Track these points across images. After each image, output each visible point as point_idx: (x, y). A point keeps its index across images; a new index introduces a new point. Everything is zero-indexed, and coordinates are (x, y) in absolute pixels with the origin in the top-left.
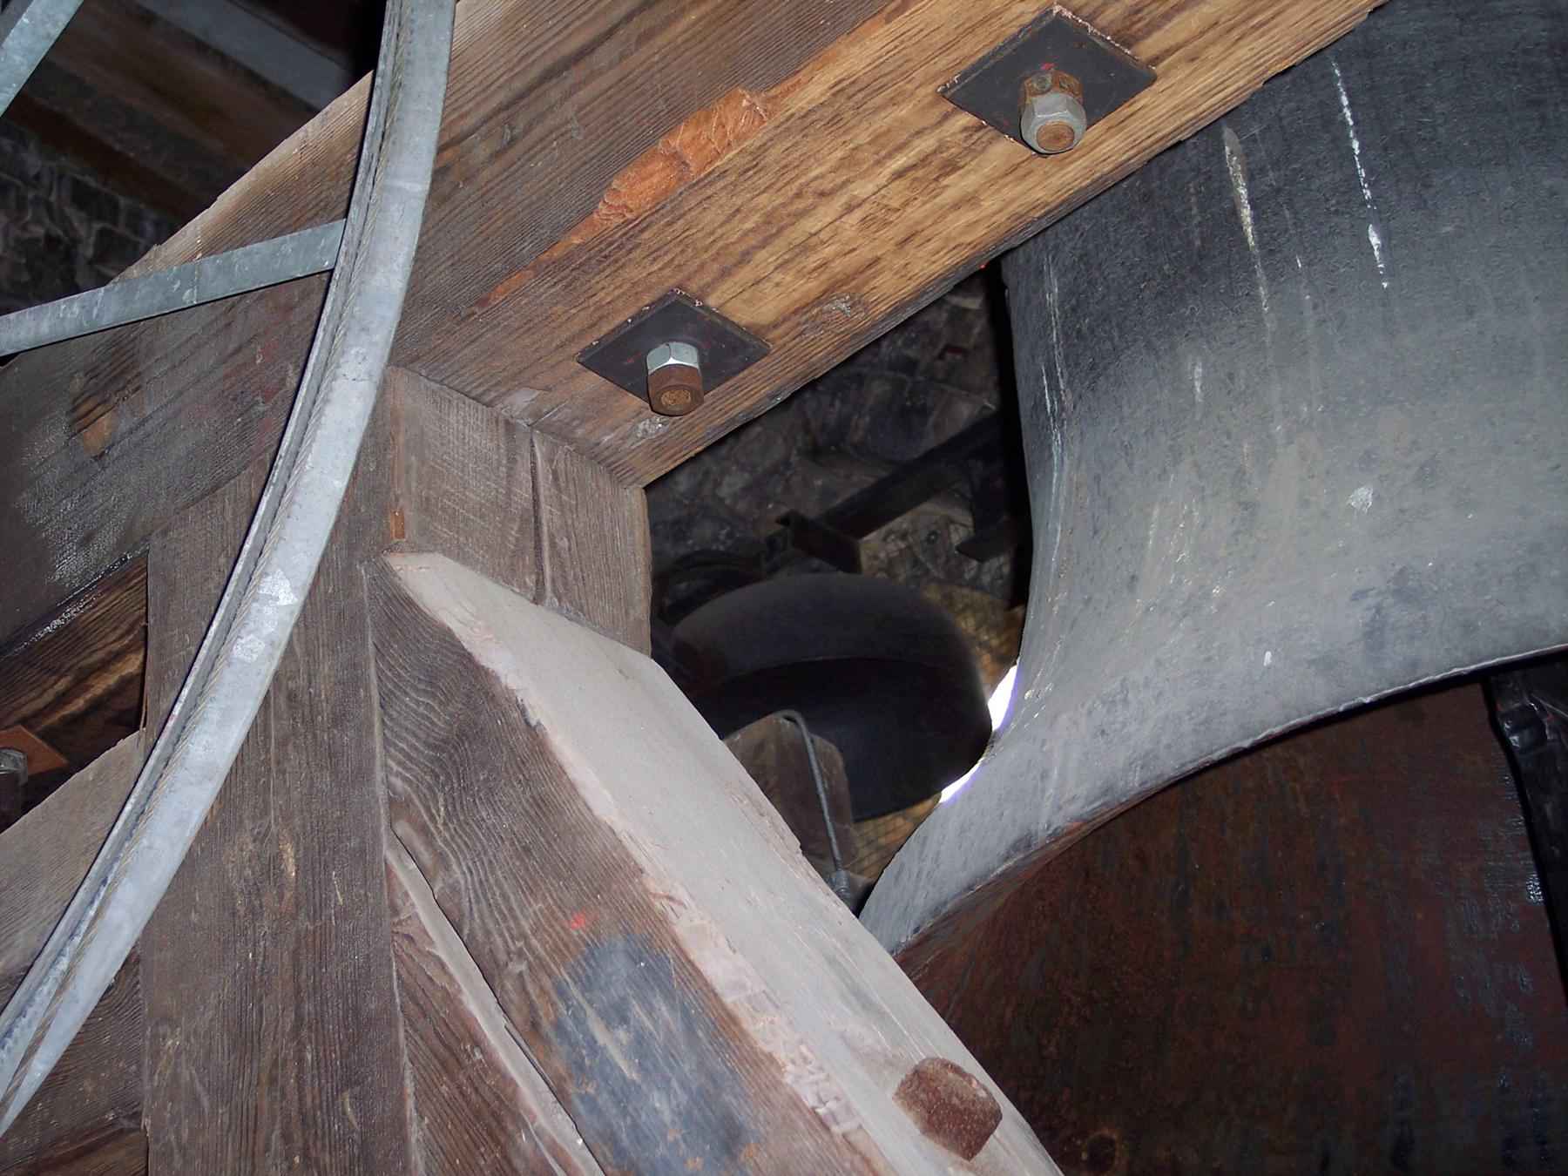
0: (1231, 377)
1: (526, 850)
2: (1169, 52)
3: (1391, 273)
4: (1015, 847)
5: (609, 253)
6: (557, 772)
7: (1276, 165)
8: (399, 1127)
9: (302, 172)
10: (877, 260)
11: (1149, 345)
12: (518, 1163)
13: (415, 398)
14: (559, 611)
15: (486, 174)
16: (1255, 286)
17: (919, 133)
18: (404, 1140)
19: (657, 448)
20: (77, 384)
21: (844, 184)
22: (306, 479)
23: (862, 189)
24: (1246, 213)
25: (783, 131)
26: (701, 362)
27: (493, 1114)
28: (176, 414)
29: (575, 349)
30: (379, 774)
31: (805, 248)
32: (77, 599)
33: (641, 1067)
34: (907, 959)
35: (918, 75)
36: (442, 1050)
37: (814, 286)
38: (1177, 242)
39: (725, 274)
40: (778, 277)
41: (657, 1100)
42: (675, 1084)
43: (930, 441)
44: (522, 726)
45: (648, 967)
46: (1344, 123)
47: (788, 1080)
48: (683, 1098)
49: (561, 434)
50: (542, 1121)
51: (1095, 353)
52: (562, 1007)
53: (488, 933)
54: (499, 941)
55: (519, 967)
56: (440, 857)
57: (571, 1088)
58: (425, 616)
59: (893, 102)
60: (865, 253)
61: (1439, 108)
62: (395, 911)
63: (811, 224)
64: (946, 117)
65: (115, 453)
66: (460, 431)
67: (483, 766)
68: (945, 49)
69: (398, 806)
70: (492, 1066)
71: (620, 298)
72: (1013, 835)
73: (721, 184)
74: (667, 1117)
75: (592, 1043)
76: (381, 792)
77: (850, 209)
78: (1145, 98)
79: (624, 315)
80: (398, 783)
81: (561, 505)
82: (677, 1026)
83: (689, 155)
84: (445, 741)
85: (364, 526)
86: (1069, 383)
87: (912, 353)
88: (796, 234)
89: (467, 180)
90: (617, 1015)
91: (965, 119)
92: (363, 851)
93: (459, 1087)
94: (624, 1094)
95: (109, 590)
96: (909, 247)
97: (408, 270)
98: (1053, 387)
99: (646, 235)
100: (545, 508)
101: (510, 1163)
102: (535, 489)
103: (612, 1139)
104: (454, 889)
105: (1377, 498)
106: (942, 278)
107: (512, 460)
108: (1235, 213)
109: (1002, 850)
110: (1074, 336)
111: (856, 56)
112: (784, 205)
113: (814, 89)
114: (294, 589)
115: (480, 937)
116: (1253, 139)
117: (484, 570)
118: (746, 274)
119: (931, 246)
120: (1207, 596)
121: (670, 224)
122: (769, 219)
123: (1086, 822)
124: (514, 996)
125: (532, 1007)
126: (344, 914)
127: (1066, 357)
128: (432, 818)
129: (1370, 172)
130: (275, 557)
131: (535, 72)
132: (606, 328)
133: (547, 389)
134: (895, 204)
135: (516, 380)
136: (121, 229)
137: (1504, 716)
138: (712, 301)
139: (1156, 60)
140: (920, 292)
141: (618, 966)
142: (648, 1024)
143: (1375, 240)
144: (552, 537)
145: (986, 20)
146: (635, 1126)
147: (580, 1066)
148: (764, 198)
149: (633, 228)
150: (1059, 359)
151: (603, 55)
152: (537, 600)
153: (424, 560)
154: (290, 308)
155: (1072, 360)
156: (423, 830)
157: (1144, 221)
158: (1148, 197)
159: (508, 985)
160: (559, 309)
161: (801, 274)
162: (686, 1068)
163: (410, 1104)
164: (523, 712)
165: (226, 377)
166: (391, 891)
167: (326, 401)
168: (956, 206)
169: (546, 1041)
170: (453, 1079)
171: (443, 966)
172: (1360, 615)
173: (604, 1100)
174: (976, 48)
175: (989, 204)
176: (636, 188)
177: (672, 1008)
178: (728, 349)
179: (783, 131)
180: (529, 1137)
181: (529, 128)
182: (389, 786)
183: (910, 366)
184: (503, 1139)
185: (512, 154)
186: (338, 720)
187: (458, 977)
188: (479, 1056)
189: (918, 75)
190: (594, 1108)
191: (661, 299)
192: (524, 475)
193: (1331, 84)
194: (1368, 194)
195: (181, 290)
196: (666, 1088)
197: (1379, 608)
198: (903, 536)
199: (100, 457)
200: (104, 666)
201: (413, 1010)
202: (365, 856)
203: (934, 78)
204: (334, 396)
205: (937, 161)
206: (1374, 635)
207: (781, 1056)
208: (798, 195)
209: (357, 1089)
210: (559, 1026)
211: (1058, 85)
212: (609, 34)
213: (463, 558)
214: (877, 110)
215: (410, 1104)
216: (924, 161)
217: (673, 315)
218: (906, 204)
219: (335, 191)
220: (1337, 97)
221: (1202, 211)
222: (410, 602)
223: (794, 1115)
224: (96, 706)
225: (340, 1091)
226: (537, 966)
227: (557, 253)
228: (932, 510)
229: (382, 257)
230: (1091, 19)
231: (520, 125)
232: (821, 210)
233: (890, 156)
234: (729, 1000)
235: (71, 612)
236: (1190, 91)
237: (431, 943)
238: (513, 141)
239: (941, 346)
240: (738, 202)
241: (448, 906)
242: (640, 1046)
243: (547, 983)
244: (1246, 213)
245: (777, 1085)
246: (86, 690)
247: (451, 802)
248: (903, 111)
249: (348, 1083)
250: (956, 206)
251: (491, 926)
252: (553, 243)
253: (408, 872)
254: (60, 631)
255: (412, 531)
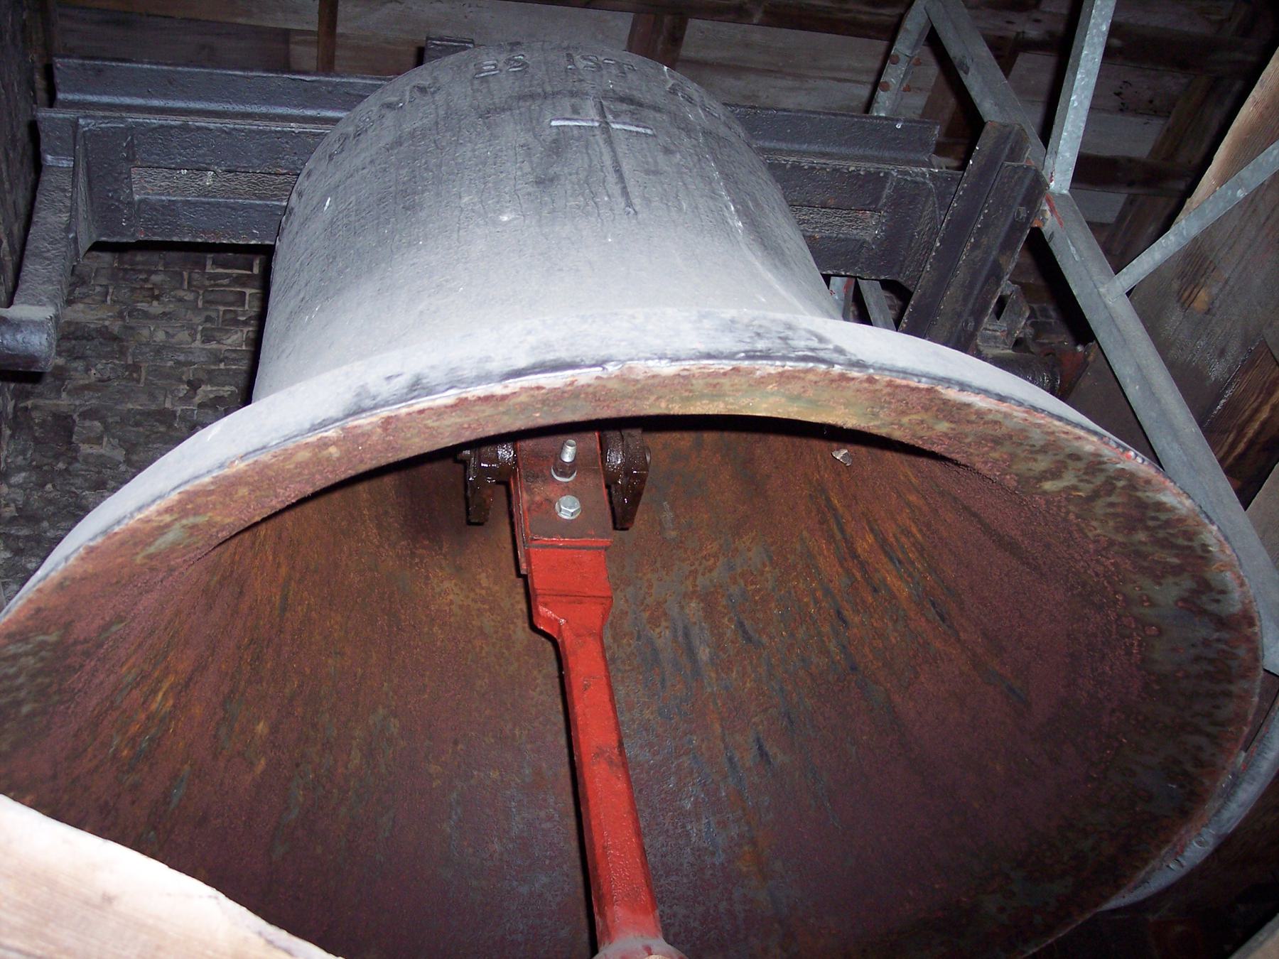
20: (1176, 286)
28: (1245, 268)
32: (1230, 384)
65: (1217, 304)
95: (1246, 372)
136: (1041, 319)
165: (1267, 235)
195: (1234, 194)
199: (1208, 312)
200: (1251, 418)
224: (1251, 443)
235: (1229, 393)
246: (1244, 436)
254: (1225, 406)
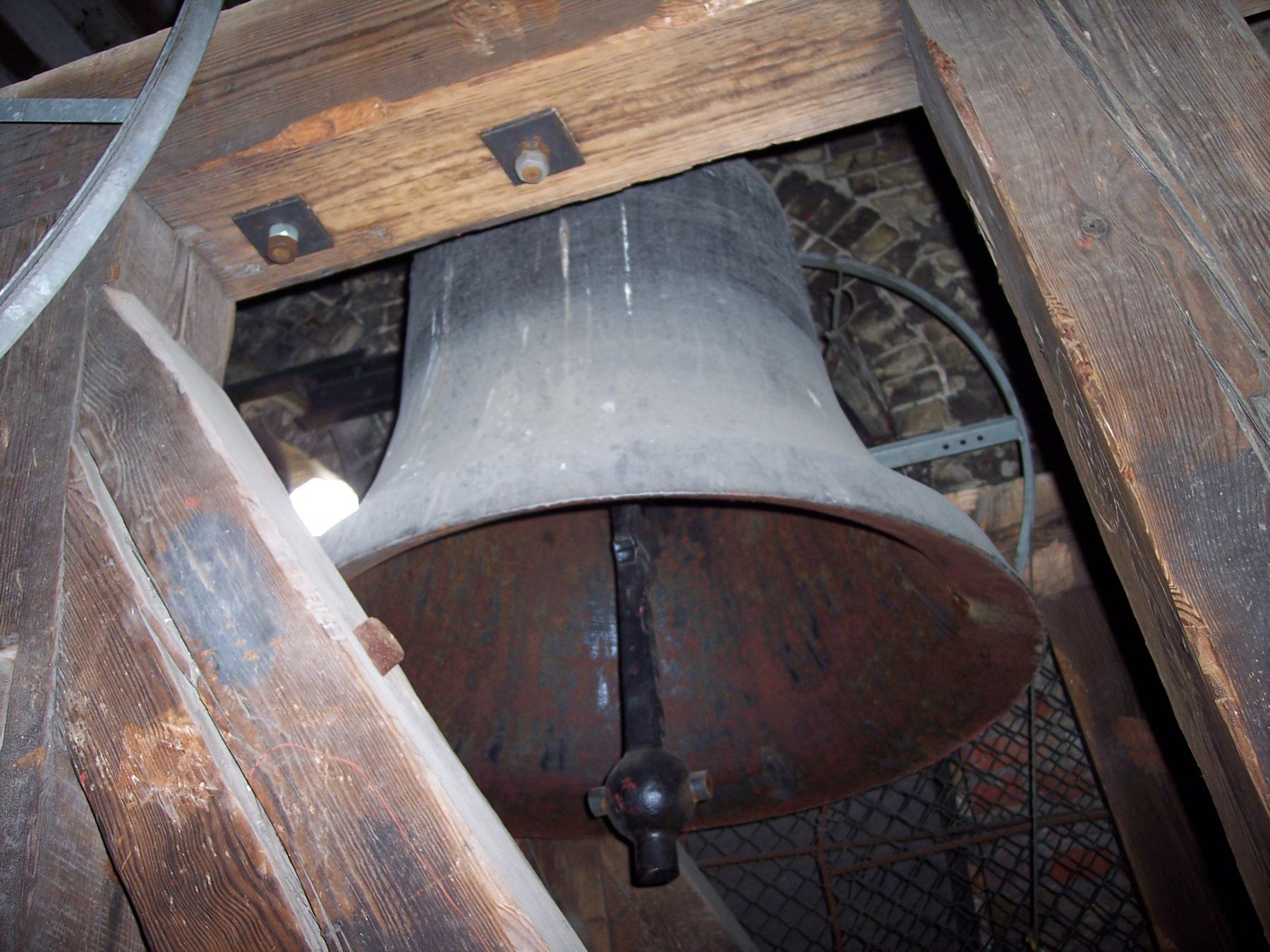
0: (544, 336)
1: (165, 458)
2: (595, 152)
3: (633, 308)
4: (407, 532)
5: (273, 163)
6: (193, 422)
7: (585, 243)
8: (50, 594)
9: (93, 76)
10: (408, 214)
11: (501, 313)
12: (127, 627)
13: (140, 212)
14: (185, 348)
15: (211, 104)
16: (563, 296)
17: (459, 152)
18: (53, 602)
19: (253, 281)
21: (411, 166)
22: (74, 229)
23: (418, 172)
24: (565, 262)
25: (392, 127)
26: (300, 237)
27: (115, 596)
29: (233, 211)
30: (76, 401)
31: (375, 195)
33: (217, 586)
34: (342, 571)
35: (472, 120)
36: (87, 556)
37: (370, 217)
38: (526, 266)
39: (329, 195)
40: (355, 206)
41: (224, 605)
42: (236, 598)
43: (291, 364)
44: (175, 392)
45: (231, 533)
46: (622, 233)
47: (308, 607)
48: (240, 606)
49: (204, 257)
50: (146, 604)
51: (468, 307)
52: (171, 546)
53: (131, 498)
54: (137, 504)
55: (146, 520)
56: (108, 454)
57: (169, 590)
58: (123, 323)
59: (453, 131)
60: (404, 208)
61: (669, 240)
62: (72, 476)
63: (384, 183)
64: (476, 148)
66: (157, 237)
67: (145, 409)
68: (492, 110)
69: (85, 420)
70: (119, 569)
71: (269, 189)
72: (406, 527)
73: (347, 145)
74: (228, 614)
75: (187, 568)
76: (75, 410)
77: (407, 181)
78: (573, 173)
79: (267, 201)
80: (88, 408)
81: (197, 295)
82: (243, 567)
83: (337, 123)
84: (124, 391)
85: (95, 269)
86: (450, 322)
87: (293, 318)
88: (373, 186)
89: (198, 104)
90: (207, 555)
91: (486, 152)
92: (56, 440)
93: (95, 579)
94: (202, 598)
96: (428, 212)
97: (162, 136)
98: (439, 322)
99: (297, 160)
100: (189, 294)
101: (121, 624)
102: (186, 282)
103: (191, 621)
104: (114, 471)
105: (617, 409)
106: (436, 235)
107: (178, 261)
108: (559, 259)
109: (398, 533)
110: (457, 300)
111: (446, 99)
112: (375, 167)
113: (417, 108)
114: (51, 287)
115: (126, 499)
116: (576, 228)
117: (154, 313)
118: (338, 199)
119: (438, 215)
120: (523, 434)
121: (313, 158)
122: (363, 173)
123: (450, 527)
124: (142, 535)
125: (152, 542)
126: (36, 472)
127: (451, 309)
128: (107, 431)
129: (632, 259)
130: (45, 267)
131: (253, 60)
132: (254, 205)
133: (208, 230)
134: (431, 186)
135: (193, 219)
137: (618, 543)
138: (316, 208)
139: (588, 154)
140: (423, 239)
141: (212, 530)
142: (225, 562)
143: (628, 291)
144: (189, 309)
145: (517, 103)
146: (207, 617)
147: (177, 579)
148: (367, 160)
149: (293, 153)
150: (446, 307)
151: (297, 61)
152: (176, 338)
153: (126, 295)
154: (69, 145)
155: (453, 311)
156: (100, 436)
157: (510, 252)
158: (514, 241)
159: (139, 528)
160: (234, 186)
161: (366, 209)
162: (245, 591)
163: (60, 582)
164: (177, 385)
166: (71, 465)
167: (97, 191)
168: (460, 198)
169: (158, 562)
170: (91, 573)
171: (97, 511)
172: (614, 457)
173: (190, 600)
174: (506, 116)
175: (476, 202)
176: (302, 133)
177: (242, 558)
178: (315, 236)
179: (392, 127)
180: (136, 611)
181: (243, 87)
182: (81, 408)
183: (289, 325)
184: (118, 610)
185: (229, 98)
186: (54, 368)
187: (106, 518)
188: (111, 563)
189: (472, 120)
190: (181, 600)
191: (290, 199)
192: (182, 271)
193: (619, 213)
194: (628, 269)
195: (12, 112)
196: (230, 598)
197: (624, 456)
198: (258, 410)
201: (72, 531)
202: (58, 445)
203: (480, 124)
204: (103, 190)
205: (461, 171)
206: (621, 467)
207: (305, 594)
208: (385, 165)
209: (26, 569)
210: (168, 556)
211: (540, 148)
212: (303, 52)
213: (144, 300)
214: (443, 132)
215: (60, 582)
216: (454, 168)
217: (295, 210)
218: (436, 188)
219: (131, 84)
220: (620, 220)
221: (543, 254)
222: (115, 314)
223: (309, 626)
225: (13, 568)
226: (160, 521)
227: (247, 154)
228: (279, 399)
229: (149, 127)
230: (566, 121)
231: (238, 84)
232: (392, 177)
233: (439, 159)
234: (278, 559)
236: (596, 176)
237: (92, 497)
238: (231, 91)
239: (307, 319)
240: (353, 157)
241: (108, 479)
242: (218, 574)
243: (164, 531)
244: (565, 262)
245: (301, 608)
247: (120, 423)
248: (456, 137)
249: (21, 565)
250: (460, 198)
251: (134, 494)
252: (246, 148)
253: (83, 457)
255: (122, 277)
